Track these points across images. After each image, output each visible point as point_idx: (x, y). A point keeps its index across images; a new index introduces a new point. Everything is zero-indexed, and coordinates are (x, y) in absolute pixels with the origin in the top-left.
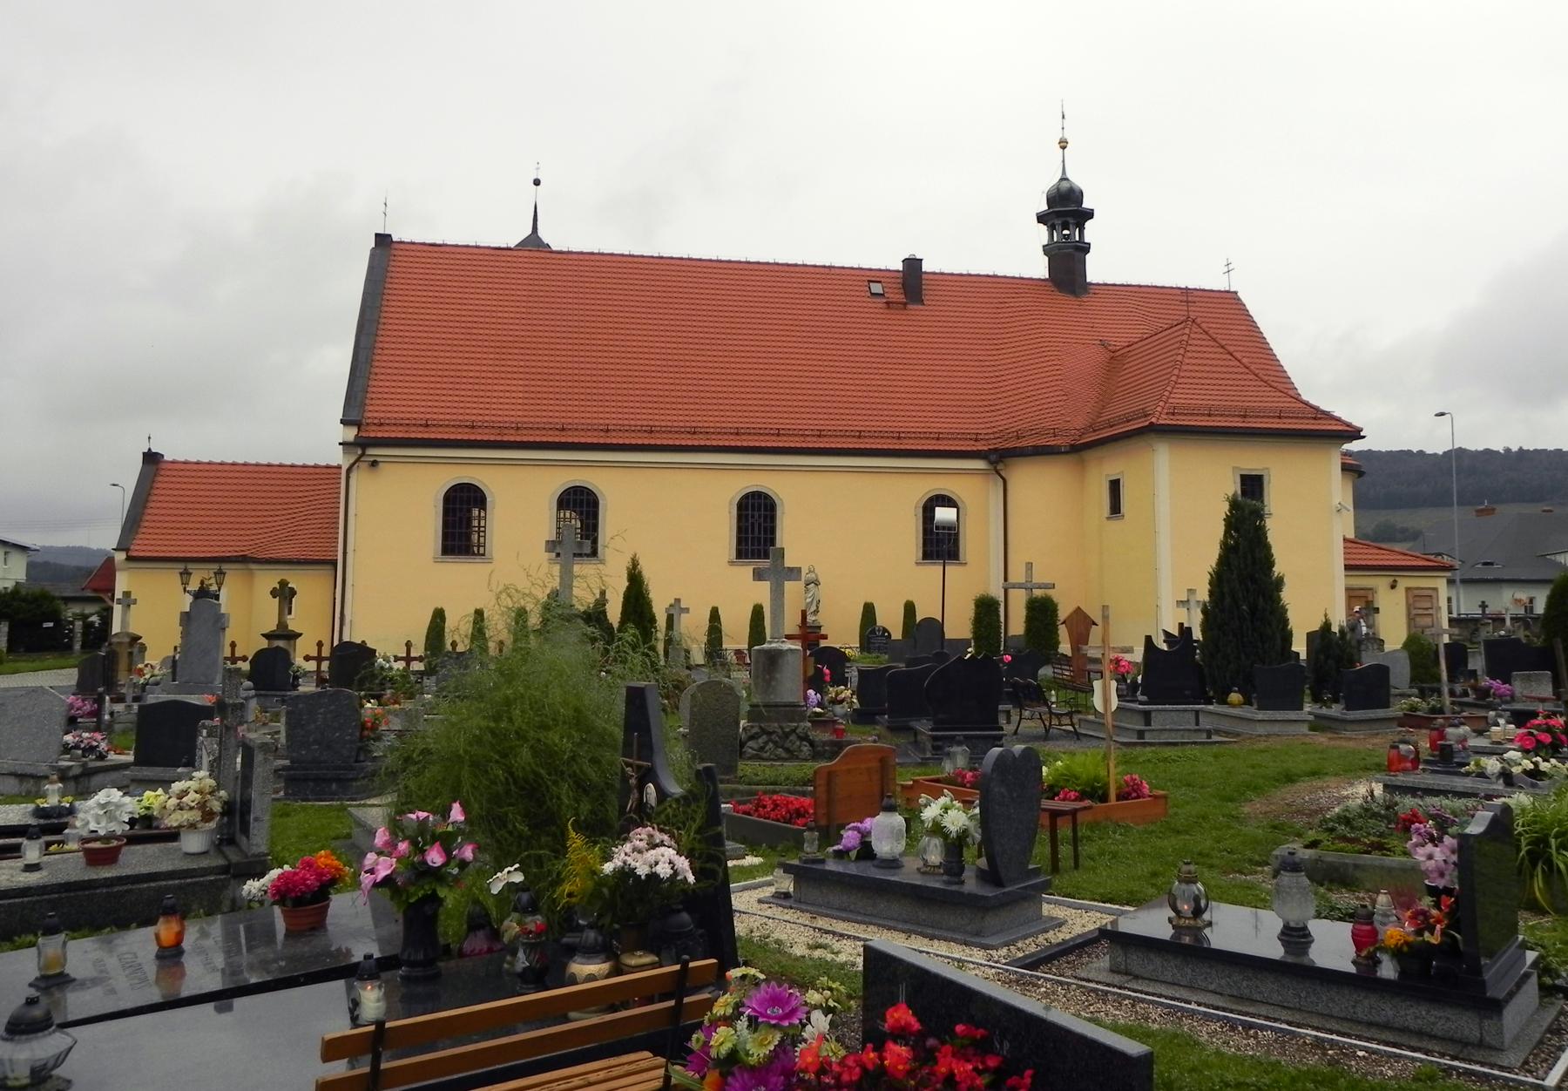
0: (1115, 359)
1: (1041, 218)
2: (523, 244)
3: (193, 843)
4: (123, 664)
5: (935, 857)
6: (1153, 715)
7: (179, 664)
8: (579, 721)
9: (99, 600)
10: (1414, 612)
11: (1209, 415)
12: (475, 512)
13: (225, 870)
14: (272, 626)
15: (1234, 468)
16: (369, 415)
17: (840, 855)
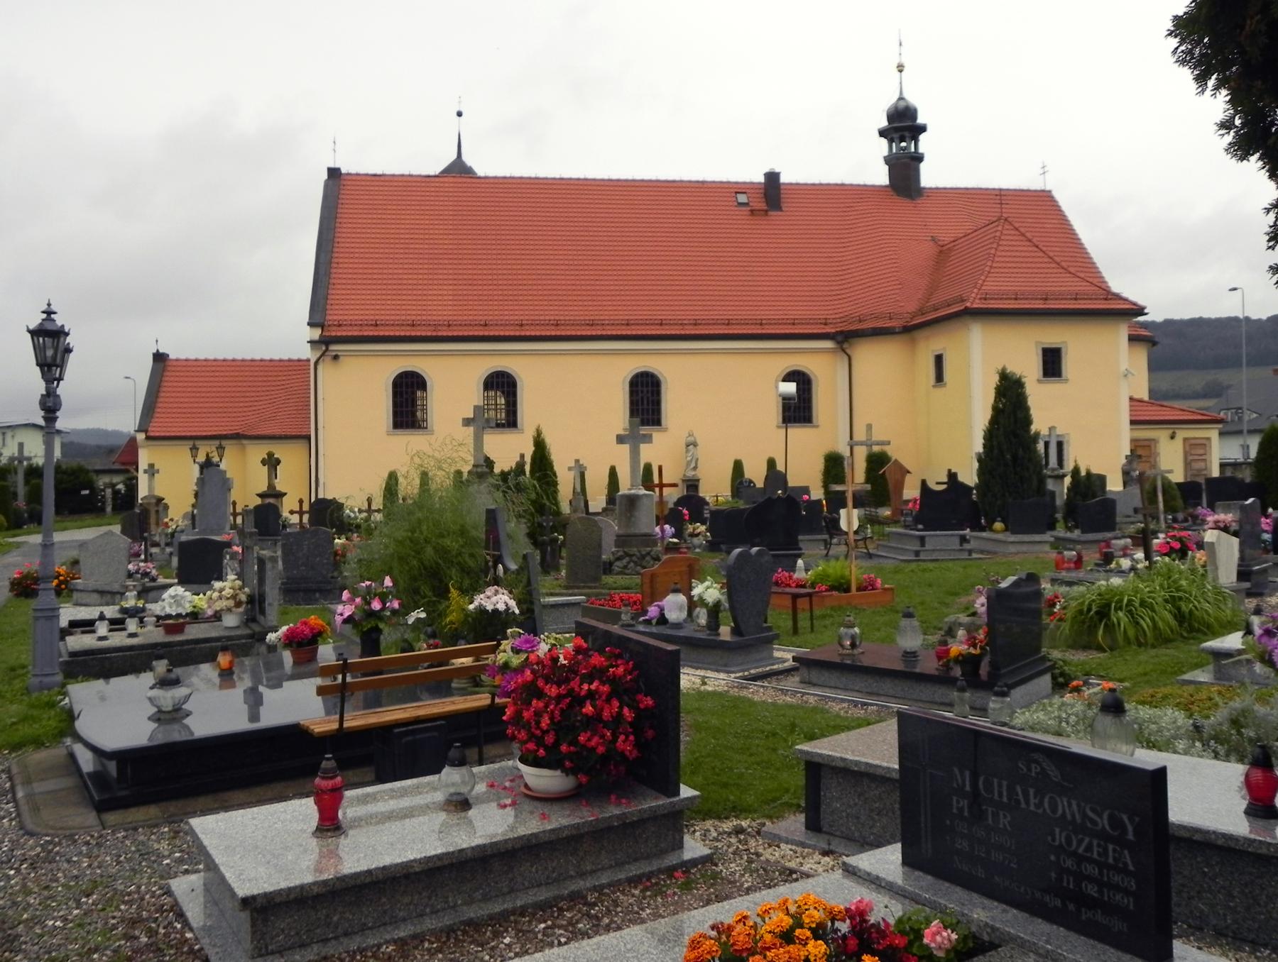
0: (943, 253)
1: (882, 133)
2: (447, 171)
3: (230, 621)
4: (153, 520)
5: (703, 620)
6: (927, 539)
7: (197, 518)
8: (463, 532)
9: (127, 471)
10: (1191, 458)
11: (1016, 299)
12: (419, 393)
13: (252, 636)
14: (263, 487)
15: (1037, 343)
16: (330, 318)
17: (648, 622)
